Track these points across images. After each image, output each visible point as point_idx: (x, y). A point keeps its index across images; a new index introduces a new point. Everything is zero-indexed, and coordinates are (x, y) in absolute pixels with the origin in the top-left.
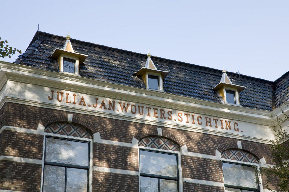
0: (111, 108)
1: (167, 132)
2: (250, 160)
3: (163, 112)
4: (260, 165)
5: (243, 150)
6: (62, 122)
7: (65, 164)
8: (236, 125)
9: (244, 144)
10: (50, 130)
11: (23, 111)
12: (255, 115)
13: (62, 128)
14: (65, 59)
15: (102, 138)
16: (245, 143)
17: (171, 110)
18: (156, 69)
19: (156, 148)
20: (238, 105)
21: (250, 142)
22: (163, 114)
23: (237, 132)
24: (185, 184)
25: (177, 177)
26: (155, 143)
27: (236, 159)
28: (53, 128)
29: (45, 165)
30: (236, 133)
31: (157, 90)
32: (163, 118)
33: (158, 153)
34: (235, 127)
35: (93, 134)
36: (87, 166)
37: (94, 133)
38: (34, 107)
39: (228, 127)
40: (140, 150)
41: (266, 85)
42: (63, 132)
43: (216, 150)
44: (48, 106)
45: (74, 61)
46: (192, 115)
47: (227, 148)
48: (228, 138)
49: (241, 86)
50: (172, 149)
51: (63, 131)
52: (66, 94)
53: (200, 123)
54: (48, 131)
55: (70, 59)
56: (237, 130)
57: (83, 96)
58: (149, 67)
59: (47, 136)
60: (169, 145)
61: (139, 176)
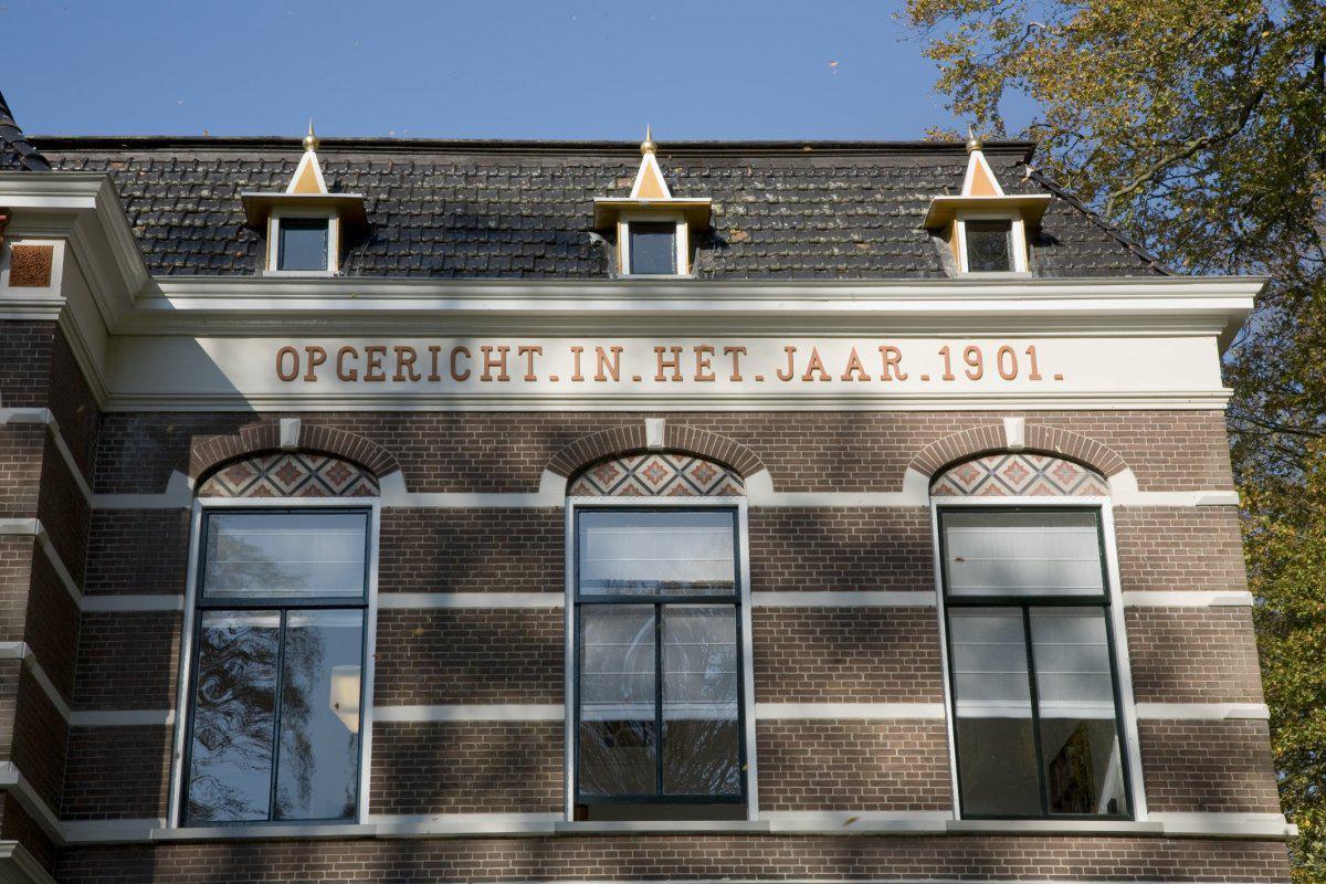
1: (1037, 427)
2: (1018, 488)
5: (304, 451)
9: (1039, 425)
11: (912, 434)
15: (1141, 489)
16: (1040, 421)
18: (999, 194)
19: (1004, 494)
20: (964, 274)
21: (839, 417)
27: (1048, 492)
28: (601, 478)
29: (1100, 592)
31: (674, 277)
32: (407, 378)
33: (289, 513)
38: (536, 415)
39: (606, 372)
42: (1048, 485)
43: (905, 468)
44: (231, 402)
52: (786, 351)
53: (346, 373)
54: (729, 490)
55: (653, 224)
57: (854, 350)
59: (579, 509)
60: (231, 480)
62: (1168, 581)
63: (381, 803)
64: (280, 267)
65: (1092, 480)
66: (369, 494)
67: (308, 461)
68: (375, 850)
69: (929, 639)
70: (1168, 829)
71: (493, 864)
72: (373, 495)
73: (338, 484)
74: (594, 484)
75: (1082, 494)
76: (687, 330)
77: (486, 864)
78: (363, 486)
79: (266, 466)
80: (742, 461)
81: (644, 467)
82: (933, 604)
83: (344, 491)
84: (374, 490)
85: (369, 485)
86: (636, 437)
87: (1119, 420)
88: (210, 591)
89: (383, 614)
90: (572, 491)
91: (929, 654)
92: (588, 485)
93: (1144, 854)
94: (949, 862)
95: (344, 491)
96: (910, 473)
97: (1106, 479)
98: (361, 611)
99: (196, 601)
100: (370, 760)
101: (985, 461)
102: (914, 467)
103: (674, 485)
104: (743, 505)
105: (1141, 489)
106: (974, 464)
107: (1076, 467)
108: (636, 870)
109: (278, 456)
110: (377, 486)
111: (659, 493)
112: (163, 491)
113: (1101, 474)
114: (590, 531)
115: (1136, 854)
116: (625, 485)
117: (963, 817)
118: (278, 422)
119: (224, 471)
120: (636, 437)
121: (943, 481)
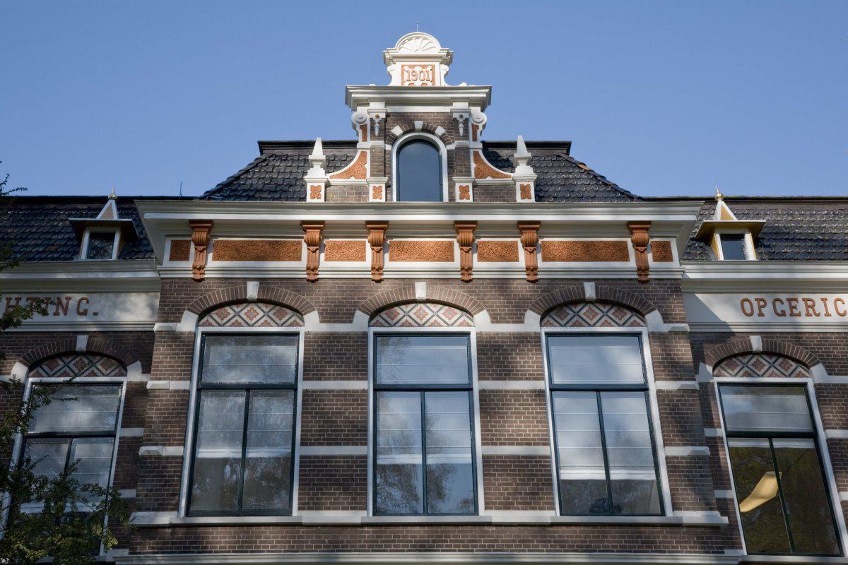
0: (60, 311)
2: (592, 323)
3: (810, 303)
4: (813, 380)
6: (744, 354)
7: (86, 432)
8: (778, 303)
10: (96, 371)
12: (120, 273)
13: (66, 365)
14: (724, 237)
17: (84, 296)
18: (735, 219)
19: (612, 326)
22: (812, 307)
23: (783, 317)
24: (831, 442)
25: (113, 429)
26: (63, 367)
27: (610, 325)
28: (559, 317)
29: (641, 381)
30: (83, 319)
34: (777, 309)
35: (126, 366)
36: (812, 431)
37: (129, 365)
40: (718, 387)
41: (46, 207)
45: (741, 237)
46: (822, 300)
47: (792, 353)
48: (696, 333)
49: (76, 219)
50: (736, 374)
51: (775, 370)
56: (85, 313)
58: (722, 219)
59: (548, 334)
61: (725, 437)
62: (522, 375)
63: (305, 504)
64: (398, 199)
65: (465, 318)
66: (298, 325)
67: (601, 307)
68: (230, 533)
69: (362, 409)
70: (494, 520)
71: (615, 542)
72: (301, 326)
73: (620, 320)
74: (554, 320)
75: (571, 326)
76: (355, 233)
77: (261, 542)
78: (635, 321)
79: (268, 310)
80: (200, 306)
81: (414, 311)
82: (543, 388)
83: (566, 324)
84: (641, 323)
85: (298, 321)
86: (241, 292)
87: (620, 284)
88: (207, 379)
89: (306, 393)
90: (543, 324)
91: (361, 417)
92: (552, 321)
93: (428, 537)
94: (626, 542)
95: (566, 324)
96: (358, 313)
97: (643, 316)
98: (467, 393)
99: (374, 385)
100: (298, 478)
101: (403, 307)
102: (360, 309)
103: (233, 321)
104: (302, 331)
105: (493, 322)
106: (396, 308)
107: (456, 310)
108: (420, 546)
109: (583, 304)
110: (303, 321)
111: (452, 325)
112: (351, 322)
113: (470, 314)
114: (213, 348)
115: (424, 537)
116: (233, 321)
117: (561, 514)
118: (246, 284)
119: (384, 312)
120: (241, 292)
121: (377, 318)
